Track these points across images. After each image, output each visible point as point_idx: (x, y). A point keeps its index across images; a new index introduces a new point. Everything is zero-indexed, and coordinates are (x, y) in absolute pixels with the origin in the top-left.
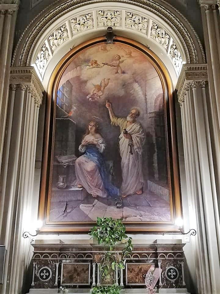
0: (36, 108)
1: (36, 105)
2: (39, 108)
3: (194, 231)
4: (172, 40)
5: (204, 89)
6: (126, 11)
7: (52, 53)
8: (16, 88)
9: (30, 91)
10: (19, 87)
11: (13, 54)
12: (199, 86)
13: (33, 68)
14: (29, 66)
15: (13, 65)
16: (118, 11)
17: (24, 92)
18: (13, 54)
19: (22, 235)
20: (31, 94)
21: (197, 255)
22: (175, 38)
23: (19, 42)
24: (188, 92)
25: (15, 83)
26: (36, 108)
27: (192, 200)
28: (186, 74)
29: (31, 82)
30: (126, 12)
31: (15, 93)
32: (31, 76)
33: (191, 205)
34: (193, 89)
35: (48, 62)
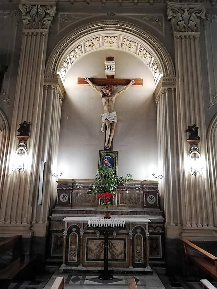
0: (60, 101)
1: (60, 99)
2: (62, 101)
3: (162, 177)
4: (153, 58)
5: (173, 93)
6: (123, 37)
7: (71, 63)
8: (48, 88)
9: (57, 90)
10: (49, 87)
11: (46, 65)
12: (170, 89)
13: (58, 75)
14: (56, 74)
15: (46, 73)
16: (116, 37)
17: (53, 90)
18: (46, 65)
19: (52, 175)
20: (57, 92)
21: (162, 187)
22: (155, 57)
23: (48, 61)
24: (163, 95)
25: (47, 84)
26: (60, 101)
27: (161, 154)
28: (162, 83)
29: (57, 84)
30: (122, 38)
31: (47, 91)
32: (57, 80)
33: (160, 161)
34: (167, 93)
35: (67, 73)
